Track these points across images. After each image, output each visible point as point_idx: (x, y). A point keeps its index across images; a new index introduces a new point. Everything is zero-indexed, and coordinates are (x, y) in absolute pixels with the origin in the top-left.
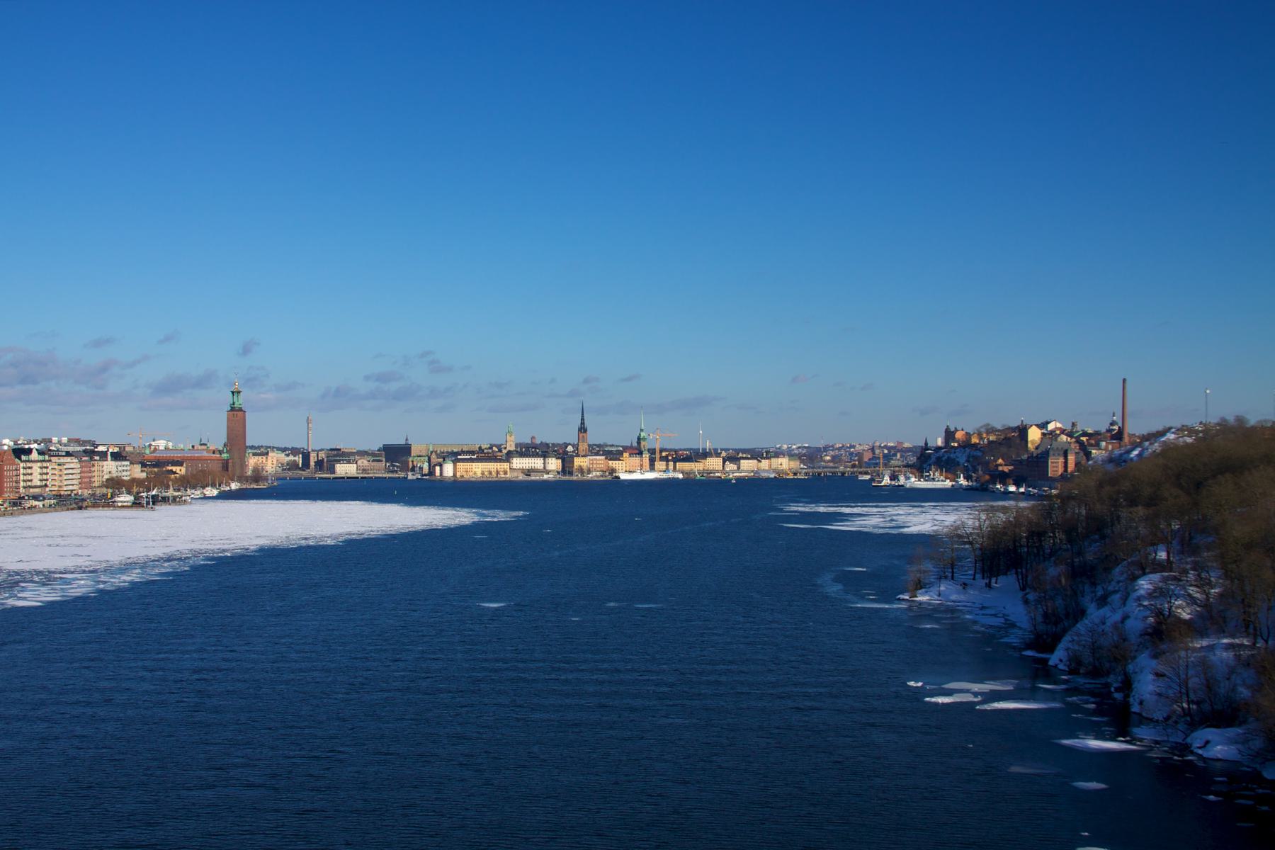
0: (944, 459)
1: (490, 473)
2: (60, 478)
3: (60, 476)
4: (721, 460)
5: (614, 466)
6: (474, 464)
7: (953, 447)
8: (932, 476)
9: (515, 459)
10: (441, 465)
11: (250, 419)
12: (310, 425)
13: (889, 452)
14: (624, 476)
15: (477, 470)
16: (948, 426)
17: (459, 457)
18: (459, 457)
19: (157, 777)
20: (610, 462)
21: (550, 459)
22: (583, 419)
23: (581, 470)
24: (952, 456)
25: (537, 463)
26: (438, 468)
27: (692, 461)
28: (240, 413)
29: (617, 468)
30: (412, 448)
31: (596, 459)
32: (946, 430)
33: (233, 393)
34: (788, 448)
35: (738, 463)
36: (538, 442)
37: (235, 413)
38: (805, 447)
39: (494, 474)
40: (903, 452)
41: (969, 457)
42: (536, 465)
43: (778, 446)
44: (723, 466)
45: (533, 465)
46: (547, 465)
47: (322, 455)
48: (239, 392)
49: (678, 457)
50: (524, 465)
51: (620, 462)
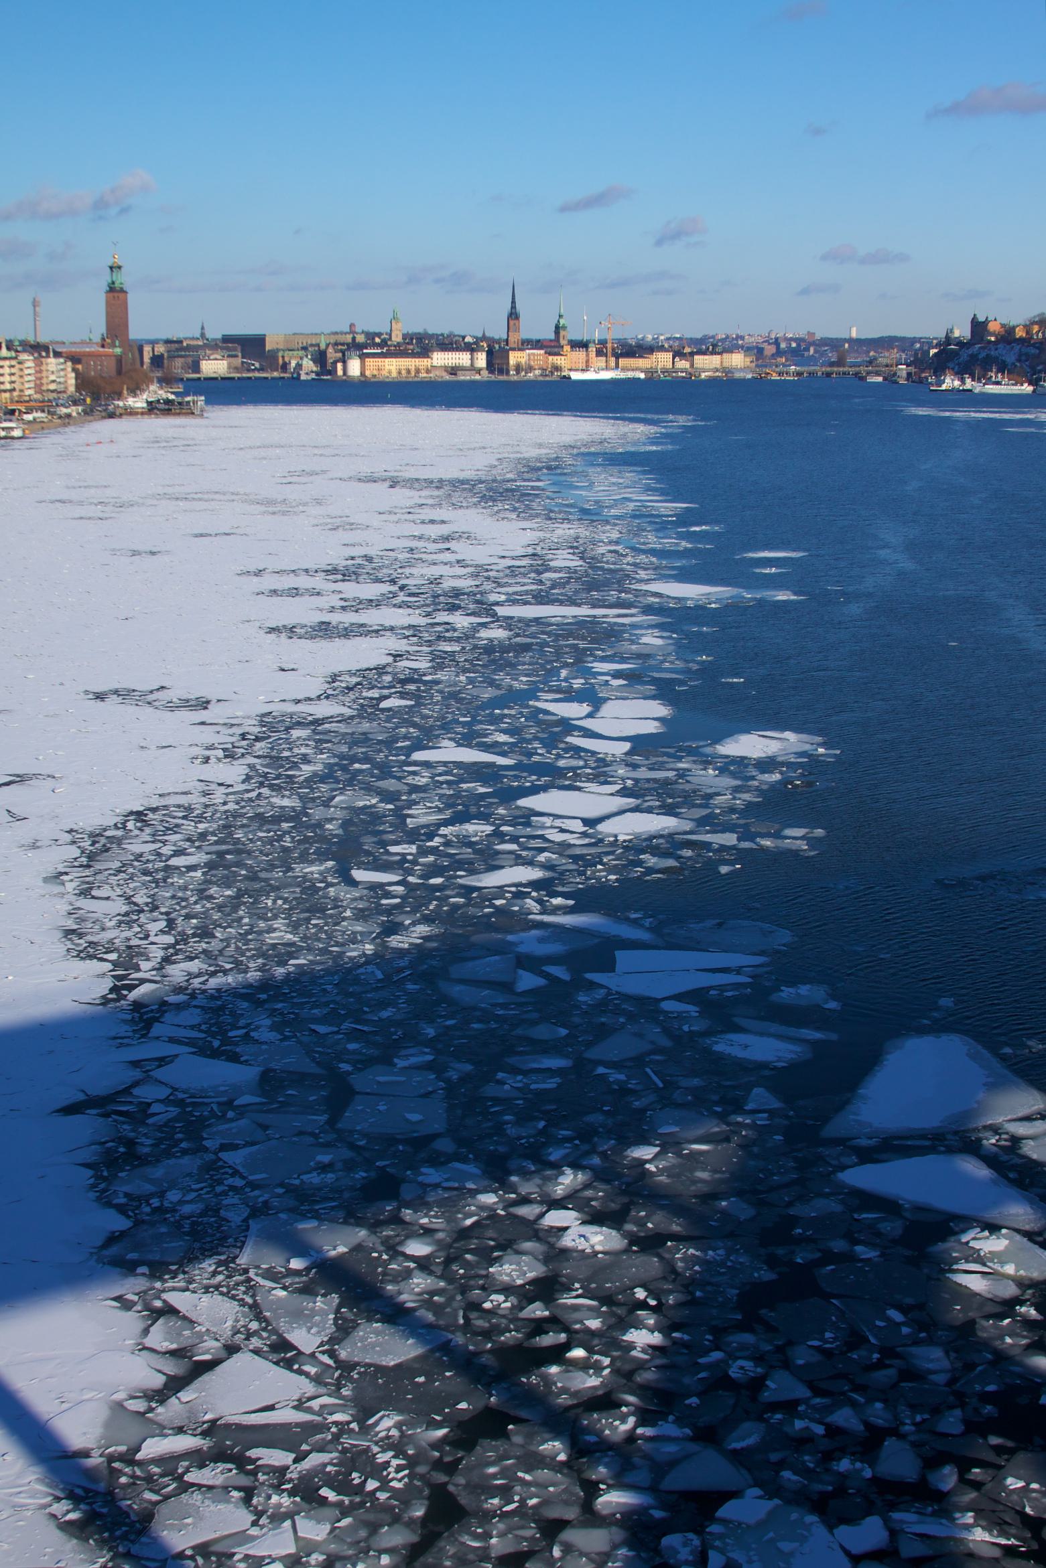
0: (980, 357)
1: (409, 371)
2: (21, 380)
3: (21, 377)
4: (670, 355)
5: (559, 362)
6: (387, 360)
7: (990, 342)
8: (993, 379)
9: (435, 353)
10: (344, 362)
11: (135, 302)
12: (37, 309)
13: (799, 345)
14: (576, 376)
15: (392, 368)
17: (365, 351)
18: (365, 351)
20: (550, 358)
22: (513, 302)
23: (518, 368)
24: (992, 353)
25: (463, 359)
26: (340, 366)
27: (635, 357)
28: (121, 295)
29: (563, 365)
30: (267, 339)
31: (534, 354)
33: (111, 268)
34: (654, 339)
36: (818, 336)
37: (116, 295)
38: (677, 338)
40: (817, 345)
41: (1020, 355)
42: (461, 362)
43: (640, 337)
44: (673, 363)
45: (457, 361)
47: (160, 349)
48: (120, 267)
50: (446, 362)
51: (563, 358)
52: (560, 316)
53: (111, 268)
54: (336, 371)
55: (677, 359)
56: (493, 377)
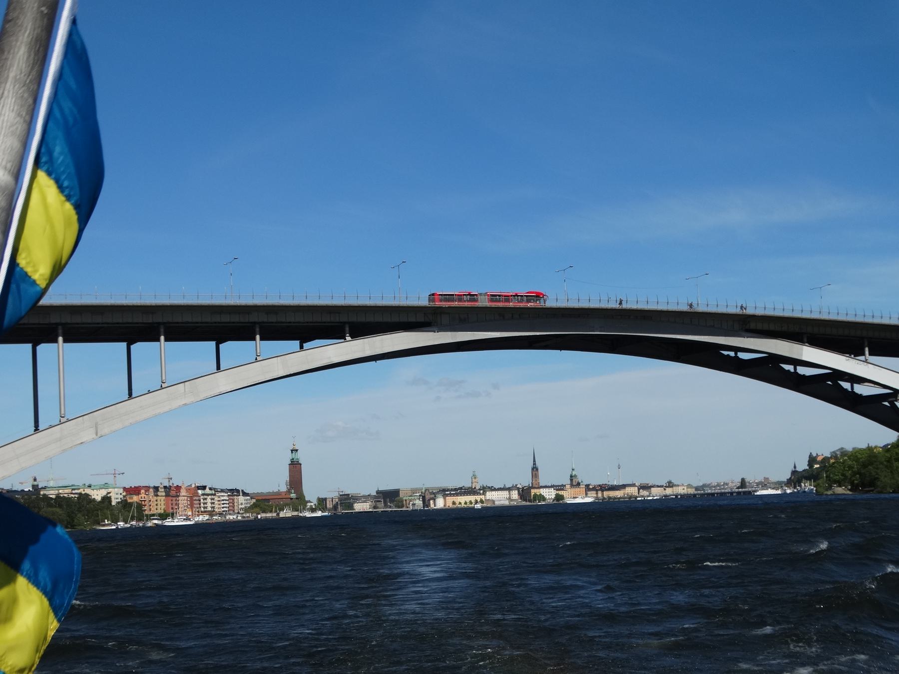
1: (460, 503)
5: (562, 494)
10: (434, 500)
16: (811, 453)
19: (714, 487)
21: (514, 491)
29: (565, 496)
32: (810, 455)
33: (292, 451)
35: (650, 490)
39: (463, 504)
46: (511, 496)
48: (297, 450)
49: (603, 488)
52: (573, 470)
53: (292, 451)
54: (430, 505)
55: (641, 491)
56: (524, 503)
